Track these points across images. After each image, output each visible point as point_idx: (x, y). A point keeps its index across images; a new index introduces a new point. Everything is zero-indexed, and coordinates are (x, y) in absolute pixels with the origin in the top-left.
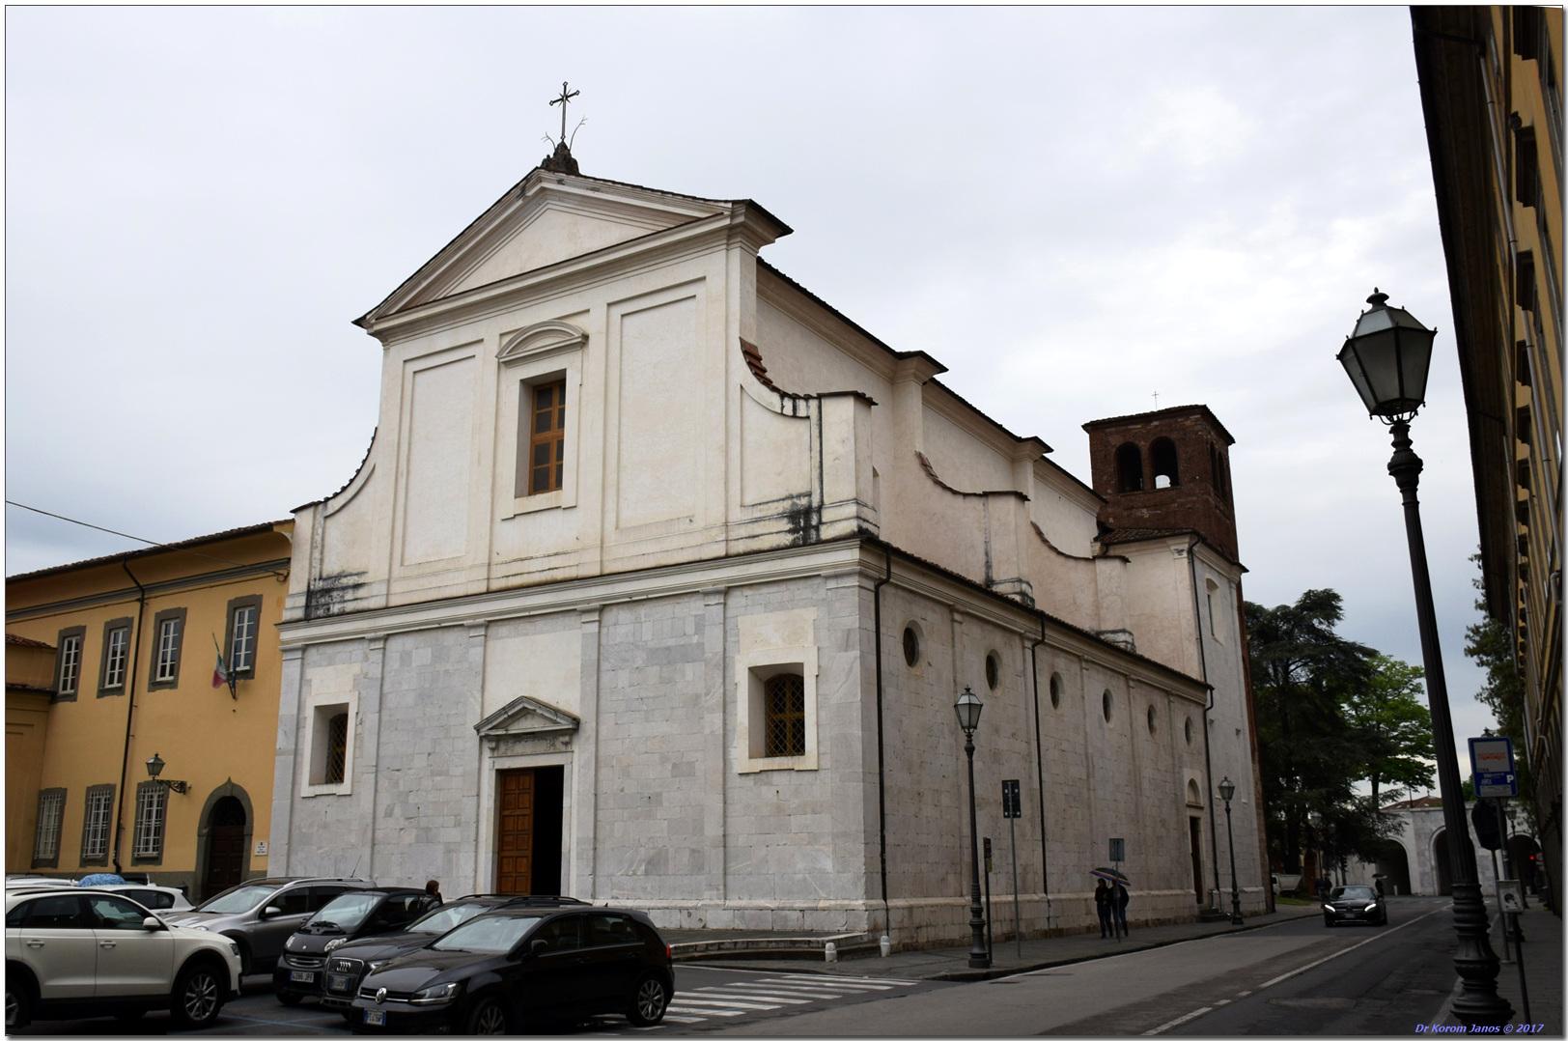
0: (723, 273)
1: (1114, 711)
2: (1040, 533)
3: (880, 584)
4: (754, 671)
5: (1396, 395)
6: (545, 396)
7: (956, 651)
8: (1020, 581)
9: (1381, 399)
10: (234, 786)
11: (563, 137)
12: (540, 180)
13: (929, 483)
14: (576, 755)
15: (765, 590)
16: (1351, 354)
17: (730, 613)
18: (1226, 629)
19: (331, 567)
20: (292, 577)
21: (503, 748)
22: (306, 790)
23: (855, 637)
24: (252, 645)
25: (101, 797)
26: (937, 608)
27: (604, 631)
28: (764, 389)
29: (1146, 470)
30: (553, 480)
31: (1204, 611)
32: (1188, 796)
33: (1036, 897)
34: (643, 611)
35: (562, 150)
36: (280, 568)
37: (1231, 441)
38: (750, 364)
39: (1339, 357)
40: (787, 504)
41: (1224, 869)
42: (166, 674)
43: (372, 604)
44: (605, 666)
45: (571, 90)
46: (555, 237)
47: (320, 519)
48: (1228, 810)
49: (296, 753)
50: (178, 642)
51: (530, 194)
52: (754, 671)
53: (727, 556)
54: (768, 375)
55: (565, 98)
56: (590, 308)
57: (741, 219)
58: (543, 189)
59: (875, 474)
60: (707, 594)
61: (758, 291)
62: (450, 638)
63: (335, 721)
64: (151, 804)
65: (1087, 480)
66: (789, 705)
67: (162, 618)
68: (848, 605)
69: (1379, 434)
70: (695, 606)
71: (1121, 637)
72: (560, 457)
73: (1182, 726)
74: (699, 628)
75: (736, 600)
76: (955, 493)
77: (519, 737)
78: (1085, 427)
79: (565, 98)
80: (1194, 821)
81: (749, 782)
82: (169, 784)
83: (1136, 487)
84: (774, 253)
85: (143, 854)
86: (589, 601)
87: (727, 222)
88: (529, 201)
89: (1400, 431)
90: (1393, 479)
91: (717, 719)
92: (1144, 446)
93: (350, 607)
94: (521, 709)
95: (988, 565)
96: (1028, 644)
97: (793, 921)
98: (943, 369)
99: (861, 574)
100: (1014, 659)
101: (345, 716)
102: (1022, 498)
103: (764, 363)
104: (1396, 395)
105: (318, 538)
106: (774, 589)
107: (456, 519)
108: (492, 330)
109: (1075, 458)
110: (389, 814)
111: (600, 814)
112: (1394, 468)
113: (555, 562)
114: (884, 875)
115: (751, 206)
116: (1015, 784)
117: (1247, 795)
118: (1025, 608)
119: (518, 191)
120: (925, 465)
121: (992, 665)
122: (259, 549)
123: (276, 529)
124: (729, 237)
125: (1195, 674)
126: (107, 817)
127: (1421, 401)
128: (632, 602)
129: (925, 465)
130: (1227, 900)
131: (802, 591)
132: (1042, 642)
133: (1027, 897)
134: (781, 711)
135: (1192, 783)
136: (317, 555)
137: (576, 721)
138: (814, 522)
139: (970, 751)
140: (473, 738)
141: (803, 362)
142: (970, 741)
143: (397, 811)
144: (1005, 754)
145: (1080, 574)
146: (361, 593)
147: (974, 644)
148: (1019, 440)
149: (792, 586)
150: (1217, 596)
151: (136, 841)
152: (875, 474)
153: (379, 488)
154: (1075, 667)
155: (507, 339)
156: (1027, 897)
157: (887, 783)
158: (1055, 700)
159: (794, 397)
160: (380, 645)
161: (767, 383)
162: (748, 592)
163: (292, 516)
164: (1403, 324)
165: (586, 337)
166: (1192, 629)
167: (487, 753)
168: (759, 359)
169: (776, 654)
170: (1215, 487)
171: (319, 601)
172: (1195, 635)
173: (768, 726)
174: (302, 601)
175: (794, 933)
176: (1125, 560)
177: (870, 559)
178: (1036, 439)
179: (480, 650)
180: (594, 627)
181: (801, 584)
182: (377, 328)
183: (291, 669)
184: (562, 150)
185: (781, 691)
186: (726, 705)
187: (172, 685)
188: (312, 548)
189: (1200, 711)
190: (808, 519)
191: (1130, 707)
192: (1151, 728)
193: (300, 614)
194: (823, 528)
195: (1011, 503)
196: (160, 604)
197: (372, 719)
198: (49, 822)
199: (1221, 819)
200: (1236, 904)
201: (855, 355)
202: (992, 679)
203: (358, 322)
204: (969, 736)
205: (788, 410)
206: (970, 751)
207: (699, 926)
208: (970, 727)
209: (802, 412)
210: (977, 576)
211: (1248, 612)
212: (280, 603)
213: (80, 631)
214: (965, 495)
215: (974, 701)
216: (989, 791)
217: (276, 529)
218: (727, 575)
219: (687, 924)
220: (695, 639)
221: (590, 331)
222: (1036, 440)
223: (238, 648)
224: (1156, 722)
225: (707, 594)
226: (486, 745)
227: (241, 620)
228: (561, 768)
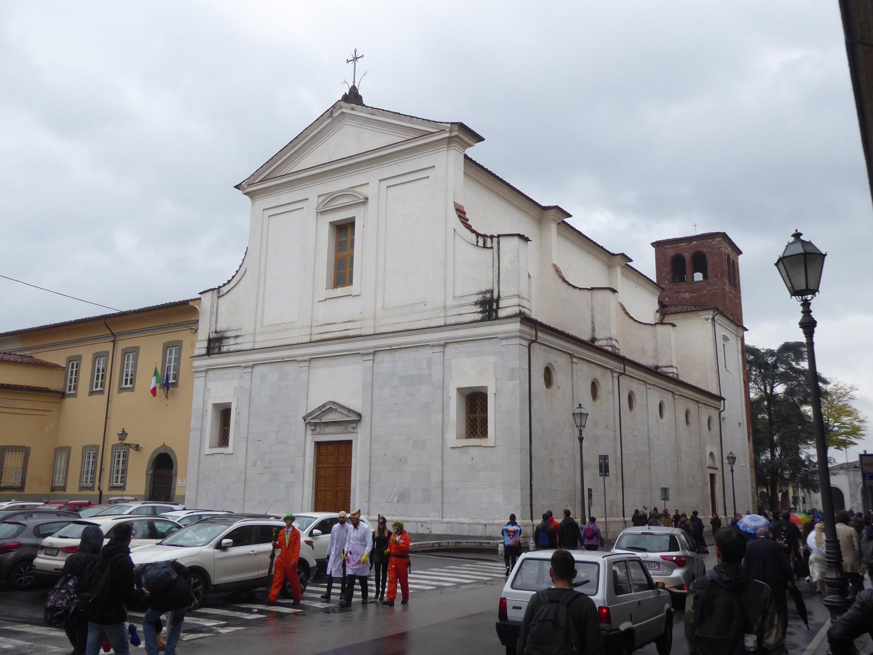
0: (447, 163)
1: (665, 413)
2: (624, 309)
4: (460, 390)
5: (804, 287)
6: (344, 230)
7: (574, 378)
8: (611, 339)
9: (797, 289)
11: (354, 82)
12: (341, 108)
14: (359, 434)
15: (466, 345)
16: (781, 264)
17: (446, 357)
18: (734, 362)
19: (221, 326)
20: (199, 331)
21: (318, 429)
24: (177, 368)
25: (92, 452)
26: (564, 355)
27: (375, 365)
29: (689, 269)
30: (347, 279)
31: (721, 355)
32: (709, 462)
33: (617, 519)
34: (397, 355)
35: (354, 90)
36: (193, 326)
37: (739, 252)
38: (459, 216)
39: (776, 265)
40: (480, 297)
41: (729, 505)
42: (129, 382)
43: (245, 347)
45: (359, 54)
46: (349, 141)
48: (732, 471)
49: (202, 430)
50: (135, 366)
51: (335, 115)
52: (460, 390)
53: (445, 326)
54: (469, 223)
55: (355, 59)
56: (369, 181)
57: (455, 133)
58: (343, 113)
59: (529, 276)
60: (433, 346)
61: (465, 173)
62: (289, 367)
63: (224, 413)
64: (119, 457)
67: (126, 352)
68: (513, 354)
69: (796, 303)
70: (427, 353)
71: (670, 370)
72: (352, 266)
74: (429, 366)
75: (450, 350)
76: (575, 287)
78: (653, 244)
79: (355, 59)
80: (712, 476)
81: (456, 452)
82: (129, 445)
83: (682, 280)
84: (475, 152)
85: (115, 484)
86: (367, 349)
87: (447, 135)
88: (334, 119)
89: (806, 305)
90: (801, 330)
91: (438, 417)
92: (687, 256)
93: (232, 348)
94: (329, 408)
95: (593, 330)
96: (616, 375)
97: (480, 531)
98: (569, 216)
99: (521, 337)
100: (607, 383)
101: (230, 409)
102: (614, 291)
103: (467, 216)
104: (804, 287)
105: (215, 309)
106: (471, 344)
107: (287, 296)
108: (313, 193)
109: (647, 263)
110: (254, 465)
111: (372, 468)
112: (802, 325)
113: (349, 326)
114: (531, 506)
115: (462, 127)
116: (605, 457)
118: (615, 356)
119: (328, 113)
120: (558, 271)
121: (594, 386)
122: (179, 314)
123: (191, 303)
124: (449, 143)
125: (714, 391)
126: (94, 463)
127: (817, 290)
128: (392, 350)
131: (487, 346)
132: (624, 374)
133: (612, 519)
134: (475, 413)
135: (711, 454)
136: (214, 319)
137: (360, 415)
138: (494, 307)
139: (581, 439)
141: (492, 215)
142: (581, 434)
143: (259, 464)
144: (600, 439)
145: (646, 332)
146: (239, 340)
147: (585, 374)
148: (613, 255)
149: (481, 342)
151: (111, 477)
152: (529, 276)
154: (643, 387)
156: (612, 519)
158: (631, 407)
159: (484, 236)
160: (250, 370)
161: (469, 227)
163: (200, 296)
164: (809, 250)
167: (309, 432)
168: (465, 213)
170: (730, 281)
171: (215, 345)
172: (715, 368)
174: (205, 344)
175: (480, 537)
176: (674, 325)
177: (526, 329)
178: (623, 255)
181: (487, 342)
182: (248, 190)
183: (199, 383)
184: (354, 90)
185: (475, 403)
186: (444, 409)
187: (131, 390)
188: (212, 314)
189: (717, 412)
190: (491, 306)
191: (676, 408)
192: (687, 422)
193: (204, 351)
194: (500, 311)
195: (609, 293)
196: (124, 344)
198: (61, 465)
199: (728, 474)
202: (594, 395)
203: (237, 187)
204: (581, 431)
205: (481, 243)
206: (581, 439)
207: (427, 532)
208: (581, 428)
209: (489, 245)
210: (586, 337)
211: (747, 350)
212: (193, 345)
213: (79, 358)
214: (580, 289)
215: (583, 411)
216: (592, 460)
217: (191, 303)
218: (444, 336)
219: (422, 531)
220: (427, 372)
221: (369, 196)
222: (623, 255)
223: (169, 369)
224: (690, 419)
225: (433, 346)
226: (309, 428)
227: (171, 354)
228: (349, 443)
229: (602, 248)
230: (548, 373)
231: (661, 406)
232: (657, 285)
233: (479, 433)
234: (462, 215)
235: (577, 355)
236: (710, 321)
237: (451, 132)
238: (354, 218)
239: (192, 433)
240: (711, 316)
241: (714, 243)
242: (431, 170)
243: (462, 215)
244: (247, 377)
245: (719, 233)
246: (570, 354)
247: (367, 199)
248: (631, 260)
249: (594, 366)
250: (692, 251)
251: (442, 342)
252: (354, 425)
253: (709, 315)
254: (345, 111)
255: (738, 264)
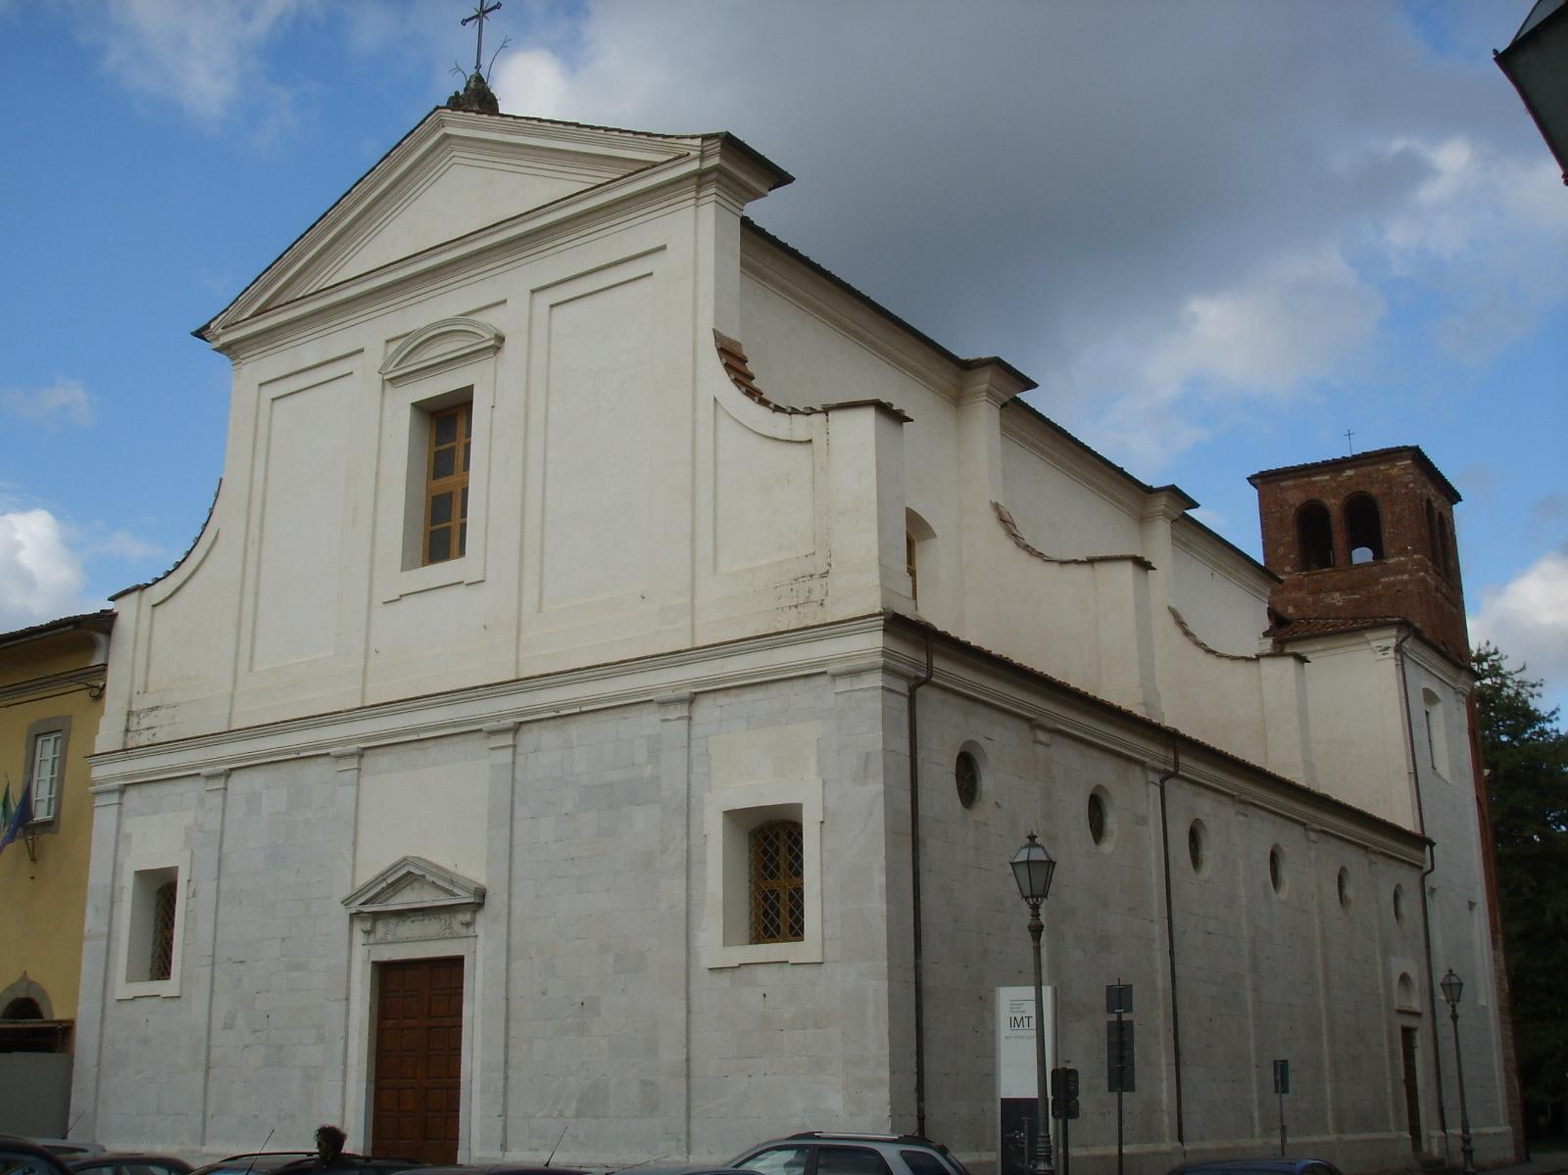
2: (1181, 623)
3: (916, 684)
6: (446, 421)
7: (1032, 785)
10: (30, 983)
11: (478, 66)
12: (441, 124)
13: (1010, 545)
14: (481, 941)
15: (748, 696)
17: (696, 732)
20: (108, 690)
22: (122, 989)
23: (878, 765)
27: (520, 760)
28: (746, 401)
29: (1339, 538)
31: (1420, 734)
34: (575, 730)
37: (1454, 497)
38: (727, 366)
44: (521, 811)
47: (146, 609)
48: (1455, 1017)
54: (755, 383)
56: (504, 295)
57: (715, 161)
58: (447, 137)
60: (663, 703)
61: (743, 264)
62: (313, 772)
65: (1259, 557)
66: (783, 866)
68: (864, 716)
70: (648, 721)
73: (1390, 897)
75: (705, 710)
77: (401, 914)
78: (1252, 480)
80: (1408, 1033)
81: (724, 980)
83: (1325, 562)
84: (769, 210)
86: (499, 717)
87: (695, 166)
94: (405, 877)
98: (1030, 385)
102: (1143, 565)
103: (750, 367)
106: (759, 694)
108: (372, 335)
110: (229, 1025)
117: (1484, 989)
124: (699, 188)
125: (1409, 824)
128: (560, 717)
129: (1005, 521)
130: (1456, 1145)
132: (1175, 775)
134: (772, 875)
140: (343, 913)
147: (1078, 772)
148: (1149, 490)
150: (1438, 712)
153: (222, 566)
154: (1229, 811)
155: (394, 346)
157: (928, 982)
158: (1196, 861)
162: (722, 700)
165: (501, 339)
166: (1402, 762)
167: (359, 937)
168: (744, 361)
169: (765, 792)
173: (753, 897)
176: (1302, 659)
177: (905, 650)
179: (352, 789)
180: (508, 754)
181: (799, 684)
183: (104, 819)
185: (771, 844)
186: (690, 866)
189: (1415, 876)
191: (1312, 865)
197: (207, 888)
200: (1468, 1153)
201: (900, 364)
203: (200, 334)
218: (692, 685)
220: (647, 771)
224: (1349, 892)
225: (663, 703)
226: (359, 927)
228: (457, 963)
229: (1120, 471)
230: (967, 768)
231: (1274, 858)
232: (1265, 574)
233: (784, 929)
234: (736, 364)
235: (1050, 724)
236: (1391, 653)
237: (702, 158)
238: (470, 389)
239: (86, 944)
240: (1392, 642)
241: (1395, 472)
242: (660, 255)
243: (736, 364)
244: (216, 800)
245: (1406, 449)
246: (1029, 720)
247: (500, 339)
248: (1194, 505)
249: (1095, 754)
250: (1345, 493)
251: (685, 692)
252: (467, 917)
253: (1389, 638)
254: (449, 130)
255: (1452, 524)
